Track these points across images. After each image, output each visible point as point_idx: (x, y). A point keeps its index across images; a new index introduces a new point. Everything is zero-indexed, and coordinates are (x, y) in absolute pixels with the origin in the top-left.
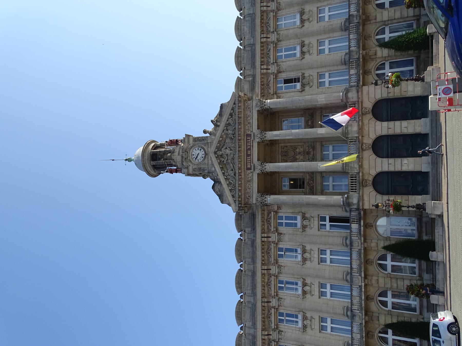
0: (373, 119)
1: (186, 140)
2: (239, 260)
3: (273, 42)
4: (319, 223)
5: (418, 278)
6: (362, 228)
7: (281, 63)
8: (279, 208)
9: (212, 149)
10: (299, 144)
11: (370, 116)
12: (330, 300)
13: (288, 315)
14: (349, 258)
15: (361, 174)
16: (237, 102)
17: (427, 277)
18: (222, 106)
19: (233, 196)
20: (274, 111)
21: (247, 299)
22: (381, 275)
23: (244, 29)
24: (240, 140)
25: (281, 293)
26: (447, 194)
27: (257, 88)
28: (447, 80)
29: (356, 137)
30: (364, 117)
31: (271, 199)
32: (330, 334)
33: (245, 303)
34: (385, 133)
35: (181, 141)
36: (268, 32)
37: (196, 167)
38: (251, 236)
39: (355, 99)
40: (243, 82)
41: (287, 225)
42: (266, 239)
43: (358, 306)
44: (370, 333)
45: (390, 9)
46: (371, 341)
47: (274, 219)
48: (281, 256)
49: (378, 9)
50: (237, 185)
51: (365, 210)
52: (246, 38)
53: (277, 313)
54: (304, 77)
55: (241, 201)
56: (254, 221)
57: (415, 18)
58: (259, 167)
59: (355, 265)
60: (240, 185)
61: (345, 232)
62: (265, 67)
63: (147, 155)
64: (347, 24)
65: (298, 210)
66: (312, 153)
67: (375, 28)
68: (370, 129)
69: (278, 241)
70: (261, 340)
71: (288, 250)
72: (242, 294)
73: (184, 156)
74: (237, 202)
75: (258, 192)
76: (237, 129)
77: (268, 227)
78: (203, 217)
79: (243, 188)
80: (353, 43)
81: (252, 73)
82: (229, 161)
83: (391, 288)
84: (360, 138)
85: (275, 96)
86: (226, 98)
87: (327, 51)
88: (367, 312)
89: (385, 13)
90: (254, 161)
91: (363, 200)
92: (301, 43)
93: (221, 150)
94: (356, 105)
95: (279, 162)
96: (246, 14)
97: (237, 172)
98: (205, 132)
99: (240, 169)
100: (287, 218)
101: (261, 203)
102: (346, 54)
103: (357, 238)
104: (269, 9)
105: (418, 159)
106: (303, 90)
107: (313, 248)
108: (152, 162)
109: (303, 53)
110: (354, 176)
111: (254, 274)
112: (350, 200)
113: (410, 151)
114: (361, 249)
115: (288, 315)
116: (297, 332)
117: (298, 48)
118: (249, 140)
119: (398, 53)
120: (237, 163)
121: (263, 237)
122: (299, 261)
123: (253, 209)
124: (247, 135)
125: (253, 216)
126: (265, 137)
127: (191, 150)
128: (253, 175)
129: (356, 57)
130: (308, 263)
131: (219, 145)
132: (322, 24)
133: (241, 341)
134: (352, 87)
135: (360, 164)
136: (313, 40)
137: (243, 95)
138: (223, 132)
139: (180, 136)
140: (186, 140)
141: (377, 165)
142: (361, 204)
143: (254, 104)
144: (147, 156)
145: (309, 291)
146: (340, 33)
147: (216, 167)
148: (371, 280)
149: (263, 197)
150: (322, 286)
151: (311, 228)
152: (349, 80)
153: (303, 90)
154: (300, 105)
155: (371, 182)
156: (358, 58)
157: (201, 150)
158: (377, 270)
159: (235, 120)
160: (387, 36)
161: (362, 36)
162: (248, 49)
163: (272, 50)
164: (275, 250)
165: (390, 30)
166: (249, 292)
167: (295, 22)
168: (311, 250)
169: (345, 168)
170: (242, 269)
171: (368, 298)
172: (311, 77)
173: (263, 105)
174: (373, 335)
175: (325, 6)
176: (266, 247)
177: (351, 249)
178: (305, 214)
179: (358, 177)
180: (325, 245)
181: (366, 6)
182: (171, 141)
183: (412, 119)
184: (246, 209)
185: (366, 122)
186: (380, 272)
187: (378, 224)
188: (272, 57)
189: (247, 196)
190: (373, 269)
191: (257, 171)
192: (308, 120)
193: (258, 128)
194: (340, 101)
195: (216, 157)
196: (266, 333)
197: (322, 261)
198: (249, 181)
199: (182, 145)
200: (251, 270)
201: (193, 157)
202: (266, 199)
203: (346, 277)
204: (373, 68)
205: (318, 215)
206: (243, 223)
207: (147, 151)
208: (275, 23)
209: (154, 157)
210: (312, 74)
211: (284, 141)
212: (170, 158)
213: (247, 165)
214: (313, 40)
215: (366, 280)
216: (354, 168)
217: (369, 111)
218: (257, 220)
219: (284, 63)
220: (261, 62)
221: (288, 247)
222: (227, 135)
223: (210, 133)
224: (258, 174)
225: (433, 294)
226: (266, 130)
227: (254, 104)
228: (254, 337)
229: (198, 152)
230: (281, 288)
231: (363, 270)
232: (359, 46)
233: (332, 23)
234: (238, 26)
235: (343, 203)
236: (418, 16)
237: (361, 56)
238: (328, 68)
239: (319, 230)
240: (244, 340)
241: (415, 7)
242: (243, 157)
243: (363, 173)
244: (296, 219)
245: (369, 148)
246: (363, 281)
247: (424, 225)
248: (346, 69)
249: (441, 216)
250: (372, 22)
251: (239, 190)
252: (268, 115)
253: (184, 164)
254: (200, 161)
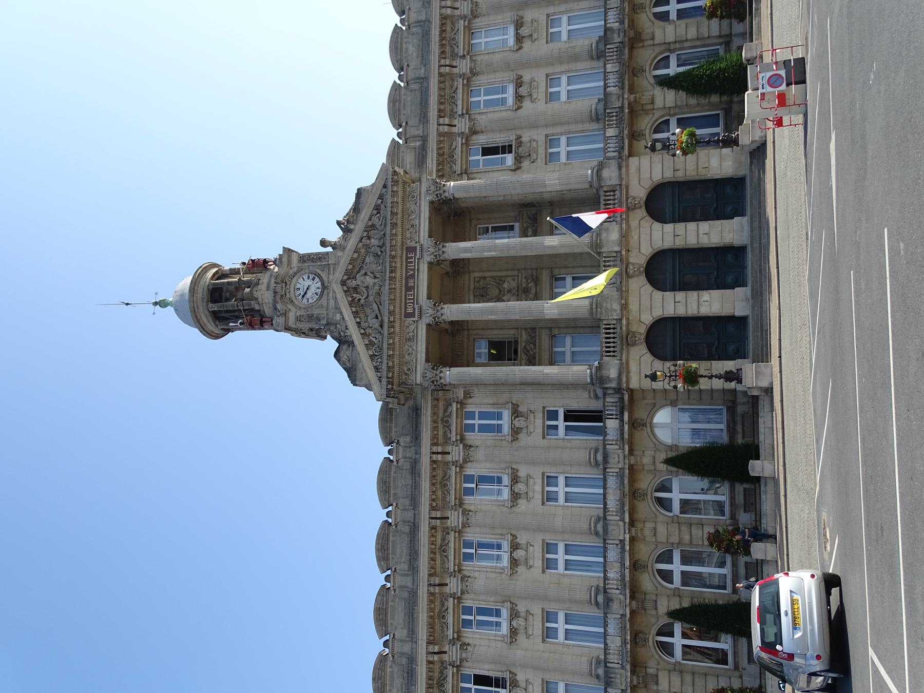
0: (648, 218)
1: (285, 260)
2: (385, 503)
3: (462, 76)
4: (544, 423)
5: (729, 521)
6: (626, 427)
7: (478, 117)
8: (468, 395)
9: (339, 274)
10: (510, 273)
11: (642, 212)
12: (564, 575)
13: (482, 611)
14: (601, 491)
15: (624, 322)
16: (389, 184)
17: (745, 519)
18: (360, 193)
19: (377, 369)
20: (464, 205)
21: (400, 581)
22: (660, 518)
23: (407, 49)
24: (393, 257)
25: (467, 566)
26: (780, 339)
27: (429, 161)
28: (776, 63)
29: (616, 252)
30: (631, 214)
31: (450, 374)
32: (563, 645)
33: (395, 590)
34: (668, 244)
35: (275, 262)
36: (454, 56)
37: (302, 312)
38: (411, 453)
39: (615, 182)
41: (483, 429)
42: (439, 457)
43: (617, 580)
44: (640, 635)
45: (678, 22)
46: (642, 651)
47: (457, 417)
48: (469, 492)
49: (656, 21)
50: (385, 346)
51: (631, 391)
52: (411, 67)
53: (460, 539)
54: (520, 143)
55: (393, 377)
56: (417, 421)
57: (721, 40)
58: (430, 311)
59: (612, 504)
60: (391, 346)
61: (593, 440)
62: (447, 121)
63: (200, 290)
64: (602, 46)
65: (505, 397)
66: (533, 291)
67: (653, 56)
68: (643, 237)
69: (465, 461)
70: (425, 662)
71: (483, 479)
72: (389, 572)
73: (278, 289)
74: (384, 380)
75: (427, 360)
76: (388, 237)
77: (445, 433)
78: (314, 417)
80: (612, 80)
81: (420, 133)
82: (371, 298)
83: (680, 543)
84: (624, 253)
85: (465, 176)
86: (368, 177)
87: (564, 97)
88: (635, 667)
89: (670, 29)
90: (420, 301)
91: (628, 372)
92: (517, 80)
94: (617, 193)
96: (411, 21)
97: (386, 320)
98: (323, 243)
99: (391, 313)
100: (483, 415)
101: (433, 382)
102: (599, 100)
103: (617, 447)
104: (457, 12)
105: (728, 292)
106: (517, 168)
107: (532, 473)
108: (210, 305)
109: (519, 98)
110: (612, 326)
111: (414, 528)
112: (604, 373)
113: (714, 349)
114: (624, 468)
115: (482, 611)
116: (499, 644)
117: (511, 89)
118: (411, 258)
119: (693, 101)
120: (387, 302)
121: (434, 453)
122: (504, 501)
123: (415, 399)
125: (416, 411)
126: (443, 252)
128: (417, 327)
129: (618, 104)
130: (522, 504)
132: (555, 105)
133: (384, 671)
134: (609, 159)
135: (623, 302)
136: (540, 75)
138: (361, 241)
139: (271, 253)
140: (285, 260)
141: (654, 304)
142: (624, 379)
143: (424, 189)
144: (201, 293)
145: (522, 559)
146: (588, 64)
147: (344, 310)
148: (641, 529)
150: (549, 548)
151: (529, 434)
152: (605, 149)
153: (517, 168)
155: (643, 337)
156: (622, 108)
157: (313, 279)
158: (653, 509)
160: (673, 69)
161: (629, 66)
162: (413, 86)
163: (460, 91)
164: (458, 479)
165: (678, 59)
166: (403, 567)
167: (505, 41)
168: (528, 612)
169: (594, 310)
170: (390, 520)
171: (636, 566)
172: (534, 144)
173: (441, 192)
174: (646, 640)
175: (561, 13)
176: (440, 472)
177: (605, 469)
178: (518, 406)
179: (619, 328)
180: (556, 465)
181: (636, 15)
183: (718, 218)
184: (402, 397)
185: (634, 223)
186: (658, 514)
187: (654, 421)
188: (460, 103)
189: (406, 369)
190: (646, 508)
191: (427, 319)
192: (527, 228)
194: (587, 186)
195: (345, 292)
196: (436, 649)
197: (550, 498)
198: (410, 339)
199: (276, 269)
200: (409, 522)
202: (442, 375)
203: (595, 526)
204: (648, 127)
205: (544, 408)
206: (396, 427)
207: (202, 282)
208: (467, 41)
209: (216, 294)
210: (535, 137)
211: (480, 260)
213: (406, 308)
214: (540, 75)
215: (633, 529)
216: (612, 310)
217: (639, 202)
218: (423, 419)
219: (483, 117)
220: (440, 111)
221: (484, 472)
222: (367, 247)
223: (335, 246)
224: (428, 325)
225: (756, 541)
226: (445, 240)
227: (424, 189)
228: (412, 659)
229: (308, 283)
230: (468, 557)
231: (626, 508)
232: (623, 84)
233: (573, 45)
234: (396, 42)
235: (592, 379)
236: (726, 36)
237: (626, 103)
238: (566, 128)
239: (544, 437)
240: (391, 667)
241: (722, 17)
242: (398, 291)
243: (628, 319)
244: (499, 416)
245: (640, 273)
246: (627, 531)
247: (739, 419)
248: (599, 130)
249: (769, 391)
250: (646, 43)
251: (389, 356)
253: (279, 306)
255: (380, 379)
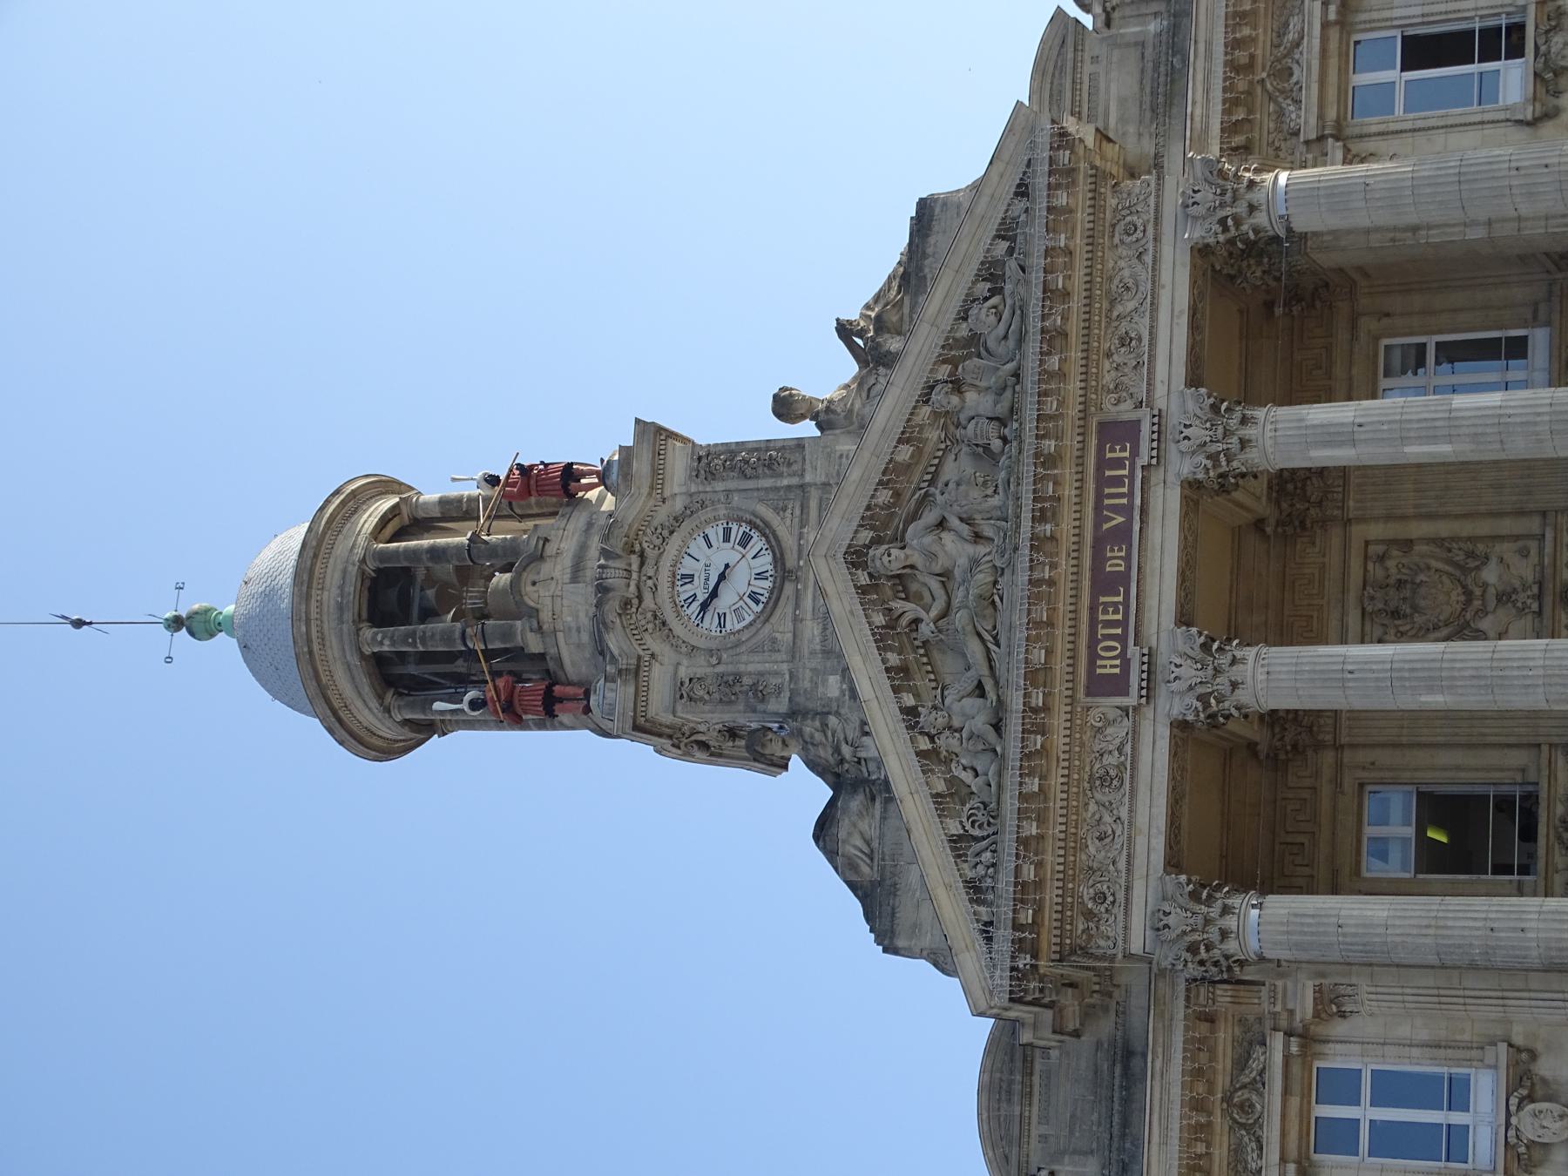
1: (641, 467)
8: (1331, 1004)
9: (840, 524)
10: (1507, 526)
16: (1041, 181)
18: (926, 215)
19: (976, 891)
20: (1325, 260)
27: (1195, 91)
31: (1264, 921)
35: (603, 477)
40: (1092, 47)
41: (1389, 1141)
47: (1286, 1091)
50: (1010, 804)
55: (1035, 925)
56: (1126, 1102)
58: (1189, 672)
60: (1034, 806)
63: (333, 578)
73: (614, 579)
74: (1003, 935)
75: (1173, 863)
77: (1237, 1152)
79: (1055, 830)
82: (960, 618)
85: (1335, 149)
86: (960, 158)
90: (1150, 629)
93: (900, 540)
95: (1343, 641)
97: (1016, 702)
98: (785, 406)
99: (1036, 676)
100: (1390, 1089)
101: (1193, 949)
108: (368, 632)
118: (1119, 463)
120: (1020, 635)
123: (1122, 1012)
124: (1102, 426)
125: (1127, 1061)
126: (1244, 443)
127: (675, 542)
128: (1135, 733)
131: (884, 496)
137: (1090, 140)
138: (925, 398)
139: (591, 441)
140: (641, 467)
147: (855, 661)
149: (1210, 900)
154: (1525, 209)
157: (745, 541)
159: (1021, 309)
173: (1241, 209)
178: (1533, 1055)
182: (525, 471)
189: (1087, 893)
191: (1173, 703)
193: (1193, 381)
195: (863, 591)
198: (1105, 780)
199: (609, 503)
201: (688, 591)
202: (1230, 922)
206: (1044, 1119)
207: (341, 549)
209: (389, 591)
212: (518, 609)
213: (1093, 657)
218: (1153, 1091)
222: (950, 420)
223: (826, 417)
226: (1250, 397)
229: (724, 554)
251: (1023, 842)
252: (1269, 306)
253: (614, 642)
254: (732, 624)
255: (987, 931)
